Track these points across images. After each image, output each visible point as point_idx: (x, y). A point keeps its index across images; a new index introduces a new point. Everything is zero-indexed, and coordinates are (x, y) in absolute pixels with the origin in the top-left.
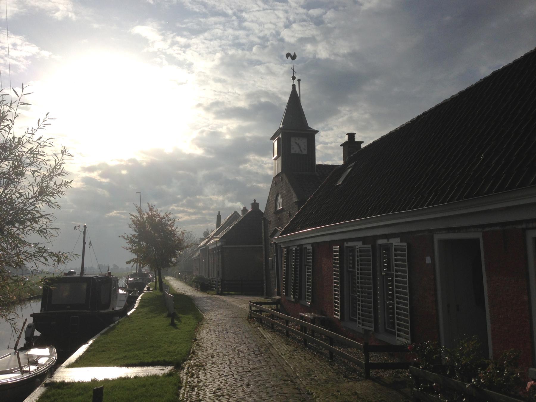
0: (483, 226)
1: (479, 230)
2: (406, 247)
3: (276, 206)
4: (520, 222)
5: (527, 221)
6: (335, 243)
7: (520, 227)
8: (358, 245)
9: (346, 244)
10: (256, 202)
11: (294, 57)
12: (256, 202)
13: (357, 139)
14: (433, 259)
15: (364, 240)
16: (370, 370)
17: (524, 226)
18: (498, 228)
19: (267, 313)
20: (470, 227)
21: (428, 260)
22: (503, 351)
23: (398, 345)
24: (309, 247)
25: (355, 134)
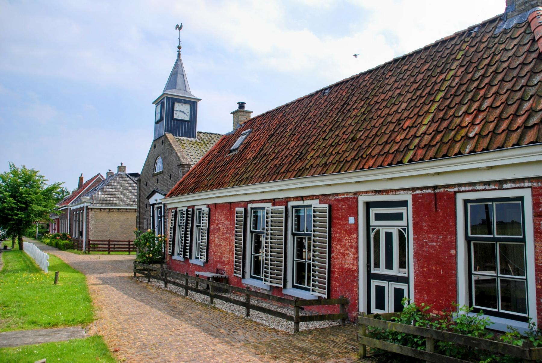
0: (413, 189)
1: (410, 192)
2: (328, 209)
3: (154, 169)
4: (454, 186)
5: (460, 185)
6: (238, 204)
7: (451, 190)
8: (269, 206)
9: (250, 206)
10: (123, 165)
11: (180, 28)
12: (123, 165)
13: (247, 108)
14: (356, 220)
15: (274, 202)
16: (426, 358)
17: (456, 189)
18: (429, 191)
19: (54, 254)
20: (398, 190)
21: (351, 220)
22: (145, 258)
23: (18, 247)
24: (205, 208)
25: (245, 103)
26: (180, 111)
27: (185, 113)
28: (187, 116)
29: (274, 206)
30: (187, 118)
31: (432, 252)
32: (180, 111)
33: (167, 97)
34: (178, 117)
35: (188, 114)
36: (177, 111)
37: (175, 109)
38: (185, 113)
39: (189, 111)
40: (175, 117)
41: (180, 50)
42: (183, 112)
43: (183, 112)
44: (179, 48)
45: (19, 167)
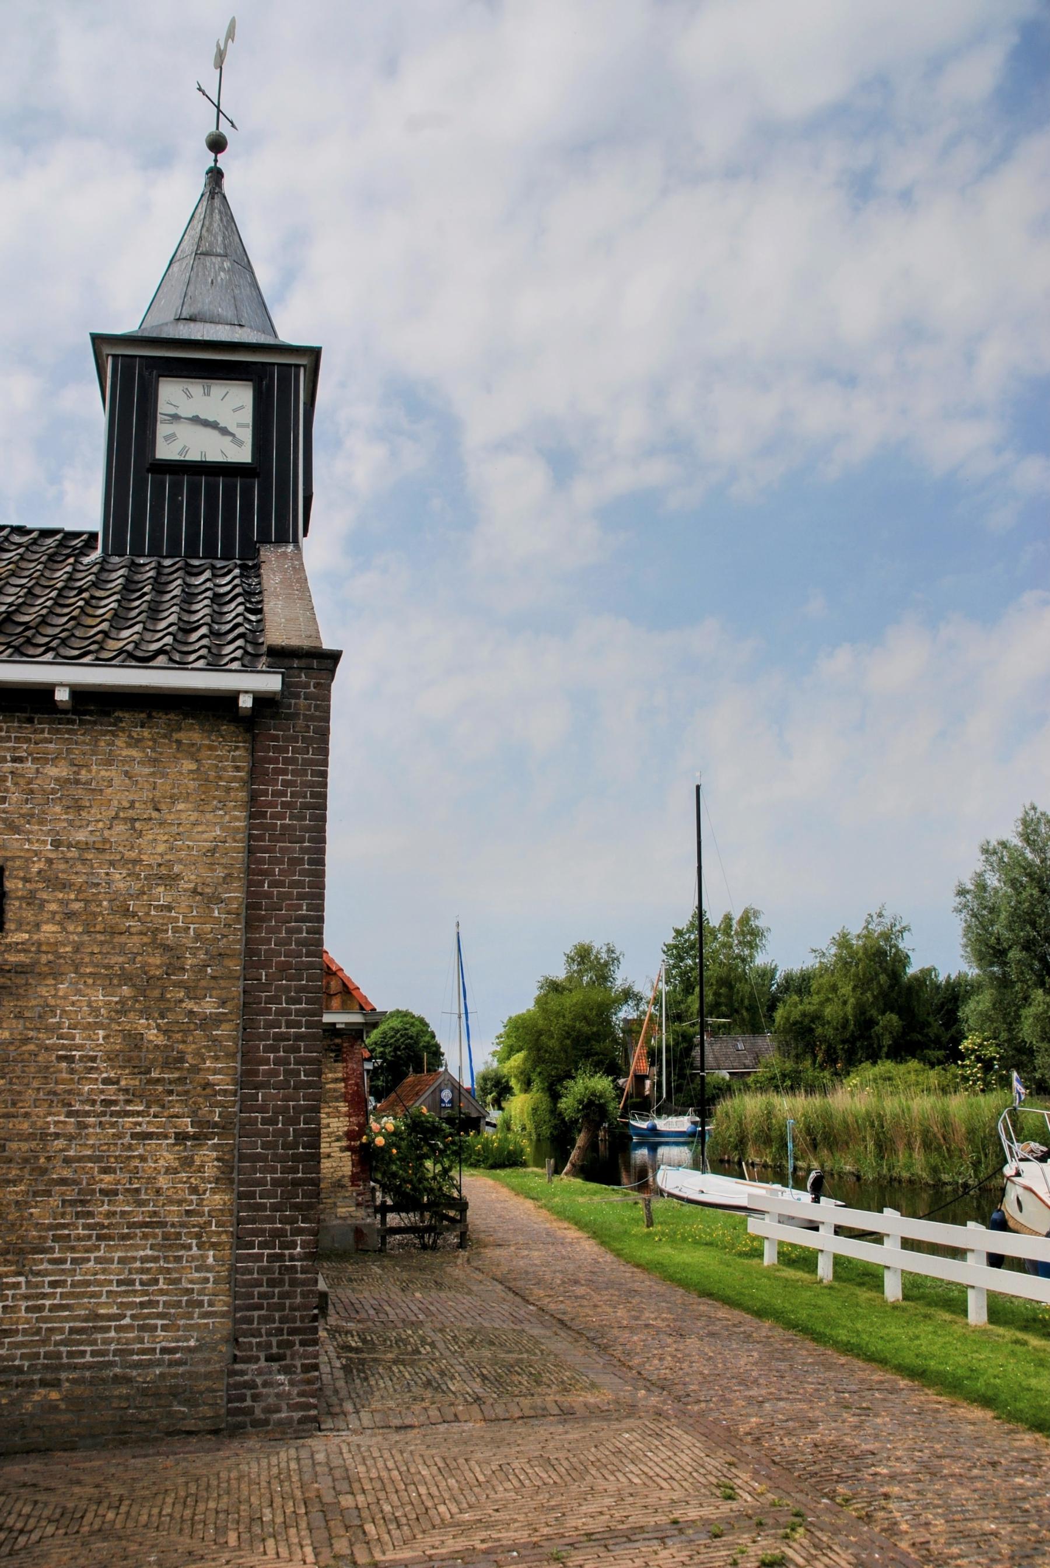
26: (196, 420)
27: (224, 431)
28: (240, 443)
29: (763, 1255)
30: (243, 454)
31: (353, 1344)
32: (196, 420)
33: (115, 356)
34: (185, 450)
35: (247, 435)
36: (175, 418)
37: (164, 407)
38: (224, 431)
39: (247, 416)
40: (166, 451)
41: (224, 160)
42: (214, 425)
43: (214, 425)
44: (217, 144)
45: (502, 1030)
